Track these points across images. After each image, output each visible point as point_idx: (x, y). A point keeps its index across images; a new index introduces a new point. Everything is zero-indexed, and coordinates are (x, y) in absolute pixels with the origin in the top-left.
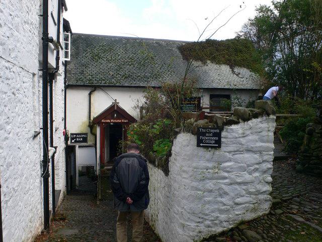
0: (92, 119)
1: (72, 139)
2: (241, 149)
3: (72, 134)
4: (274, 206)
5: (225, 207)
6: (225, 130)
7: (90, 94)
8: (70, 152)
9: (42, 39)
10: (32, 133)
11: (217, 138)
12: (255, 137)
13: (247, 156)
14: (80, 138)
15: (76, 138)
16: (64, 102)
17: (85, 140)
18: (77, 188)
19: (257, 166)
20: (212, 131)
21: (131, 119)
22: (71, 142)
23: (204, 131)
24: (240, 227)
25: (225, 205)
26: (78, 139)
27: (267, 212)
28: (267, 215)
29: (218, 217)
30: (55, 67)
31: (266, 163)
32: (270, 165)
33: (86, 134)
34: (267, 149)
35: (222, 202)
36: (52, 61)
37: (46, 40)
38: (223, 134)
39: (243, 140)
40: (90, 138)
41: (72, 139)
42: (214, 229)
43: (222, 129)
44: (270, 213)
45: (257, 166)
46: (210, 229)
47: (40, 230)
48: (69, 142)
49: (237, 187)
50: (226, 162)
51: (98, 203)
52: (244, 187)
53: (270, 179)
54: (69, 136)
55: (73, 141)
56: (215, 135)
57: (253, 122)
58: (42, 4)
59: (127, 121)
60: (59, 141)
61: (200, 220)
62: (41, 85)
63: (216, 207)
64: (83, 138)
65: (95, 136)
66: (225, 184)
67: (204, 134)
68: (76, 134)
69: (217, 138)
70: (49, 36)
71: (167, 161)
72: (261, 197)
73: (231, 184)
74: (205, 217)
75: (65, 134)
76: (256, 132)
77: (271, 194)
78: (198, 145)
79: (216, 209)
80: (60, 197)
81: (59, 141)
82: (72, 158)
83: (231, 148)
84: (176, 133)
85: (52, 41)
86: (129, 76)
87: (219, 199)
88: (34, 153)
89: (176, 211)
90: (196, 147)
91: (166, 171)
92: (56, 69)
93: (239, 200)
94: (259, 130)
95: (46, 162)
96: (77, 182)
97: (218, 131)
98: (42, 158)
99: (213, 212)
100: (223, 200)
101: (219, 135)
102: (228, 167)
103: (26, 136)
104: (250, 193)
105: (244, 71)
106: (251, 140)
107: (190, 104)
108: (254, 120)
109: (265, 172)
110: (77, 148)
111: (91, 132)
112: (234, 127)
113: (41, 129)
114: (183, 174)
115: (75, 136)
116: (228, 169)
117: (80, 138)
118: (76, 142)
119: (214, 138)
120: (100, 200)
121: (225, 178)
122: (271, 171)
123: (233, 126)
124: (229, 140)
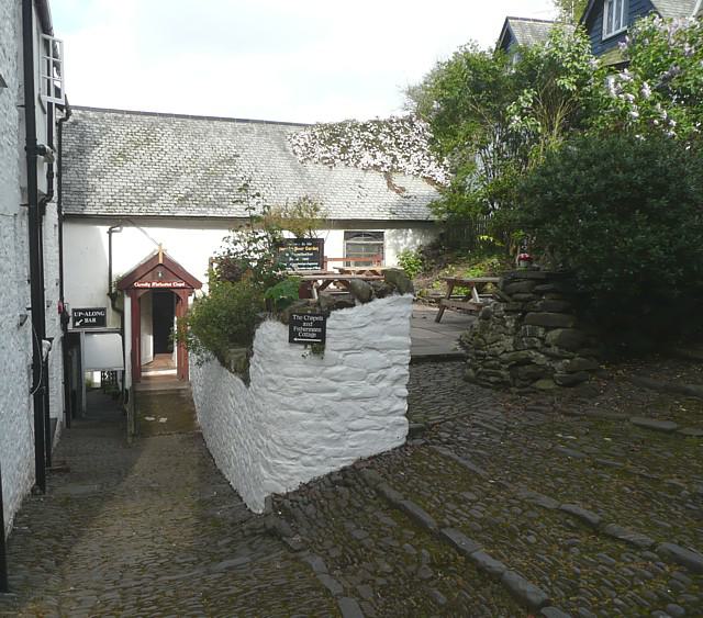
0: (114, 279)
1: (76, 320)
2: (358, 347)
3: (74, 310)
4: (412, 434)
5: (333, 435)
6: (332, 316)
7: (110, 232)
8: (71, 343)
9: (26, 149)
10: (17, 319)
11: (320, 330)
12: (379, 328)
13: (369, 355)
14: (92, 317)
15: (83, 317)
16: (58, 249)
17: (101, 321)
18: (84, 415)
19: (383, 372)
20: (313, 318)
21: (193, 284)
22: (74, 326)
23: (300, 318)
24: (357, 467)
25: (333, 431)
26: (86, 320)
27: (400, 443)
28: (400, 447)
29: (322, 450)
30: (46, 192)
31: (398, 367)
32: (405, 370)
33: (104, 310)
34: (399, 346)
35: (329, 428)
36: (42, 186)
37: (32, 151)
38: (329, 323)
39: (360, 333)
40: (111, 316)
41: (76, 320)
42: (315, 469)
43: (326, 316)
44: (406, 445)
45: (383, 372)
46: (310, 468)
47: (29, 486)
48: (70, 327)
49: (350, 403)
50: (335, 365)
51: (130, 440)
52: (363, 404)
53: (405, 392)
54: (70, 314)
55: (78, 324)
56: (316, 324)
57: (378, 304)
58: (22, 83)
59: (183, 285)
60: (53, 327)
61: (297, 455)
62: (26, 230)
63: (319, 434)
64: (97, 317)
65: (121, 313)
66: (333, 399)
67: (299, 324)
68: (84, 311)
69: (320, 330)
70: (38, 143)
71: (247, 364)
72: (392, 419)
73: (343, 399)
74: (304, 451)
75: (62, 311)
76: (382, 320)
77: (407, 415)
78: (291, 341)
79: (318, 437)
80: (57, 431)
81: (53, 327)
82: (75, 359)
83: (342, 345)
84: (262, 320)
85: (43, 151)
86: (187, 196)
87: (325, 422)
88: (18, 354)
89: (260, 444)
90: (287, 344)
91: (247, 381)
92: (47, 196)
93: (355, 424)
94: (388, 317)
95: (39, 368)
96: (84, 404)
97: (321, 319)
98: (30, 361)
99: (314, 442)
100: (329, 423)
101: (322, 325)
102: (338, 373)
103: (10, 327)
104: (374, 414)
105: (130, 384)
106: (373, 333)
107: (304, 251)
108: (378, 301)
109: (396, 381)
110: (83, 336)
111: (113, 306)
112: (345, 311)
113: (28, 309)
114: (270, 384)
115: (81, 314)
116: (337, 377)
117: (92, 317)
118: (83, 325)
119: (316, 330)
120: (133, 435)
121: (334, 391)
122: (407, 379)
123: (344, 310)
124: (337, 332)
